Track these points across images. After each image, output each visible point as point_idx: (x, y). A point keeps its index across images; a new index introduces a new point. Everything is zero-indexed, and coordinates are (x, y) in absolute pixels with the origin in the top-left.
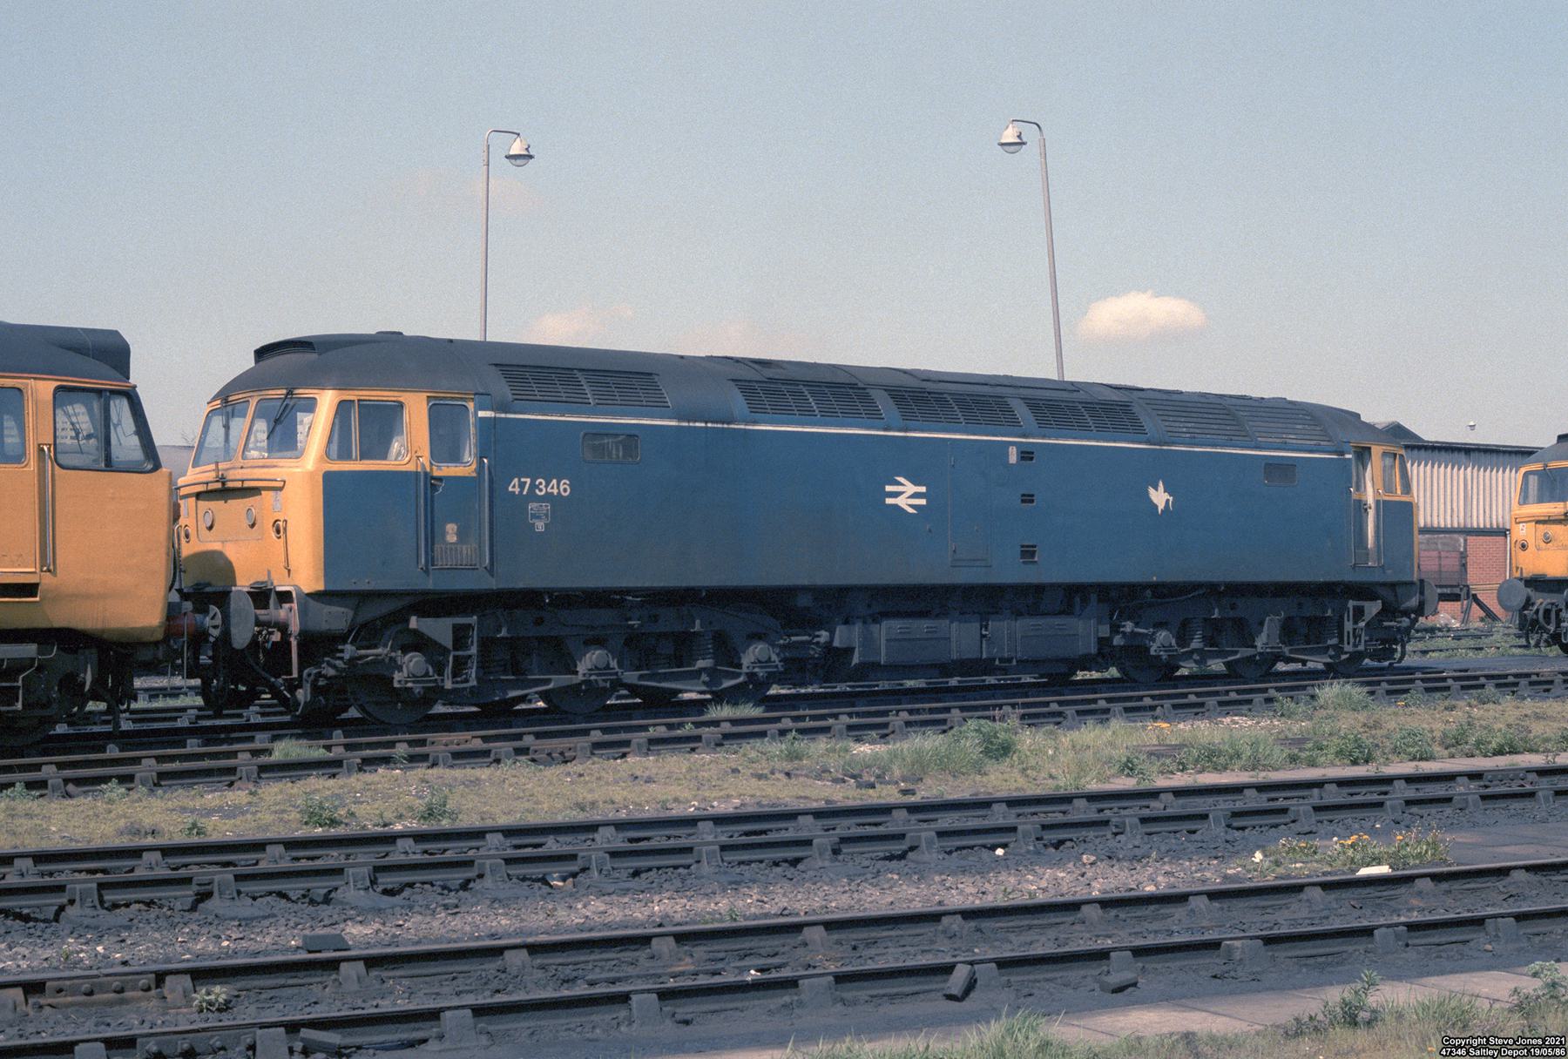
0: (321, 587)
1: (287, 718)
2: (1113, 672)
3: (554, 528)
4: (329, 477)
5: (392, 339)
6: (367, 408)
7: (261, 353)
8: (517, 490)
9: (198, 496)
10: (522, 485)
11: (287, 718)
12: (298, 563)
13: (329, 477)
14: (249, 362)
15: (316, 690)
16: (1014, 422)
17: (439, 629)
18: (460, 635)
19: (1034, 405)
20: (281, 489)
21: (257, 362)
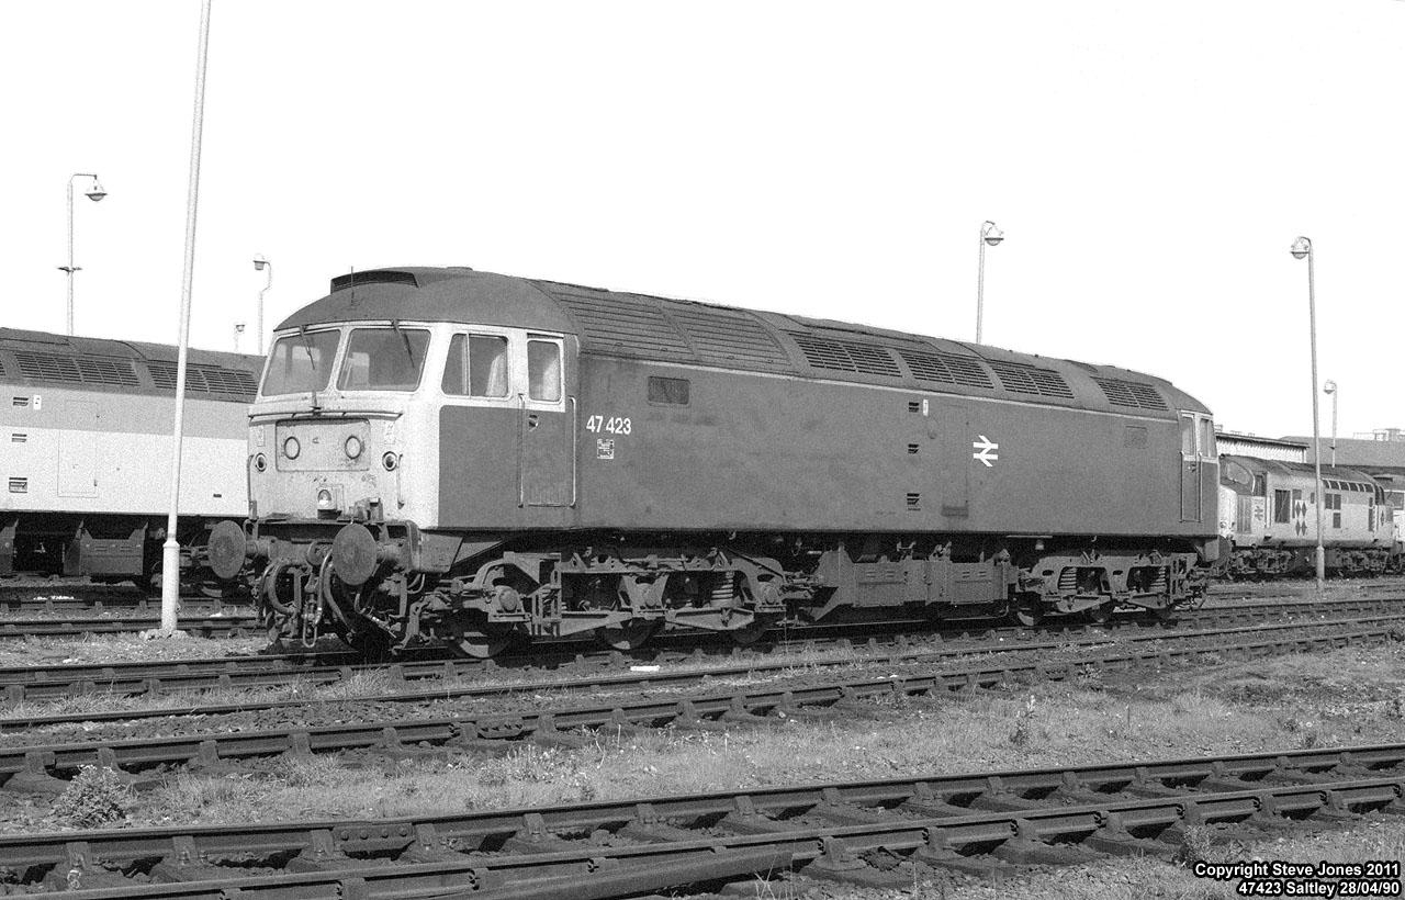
0: (436, 525)
1: (250, 646)
2: (253, 571)
3: (623, 467)
4: (446, 412)
5: (460, 276)
6: (475, 340)
7: (339, 283)
8: (593, 428)
9: (278, 423)
10: (597, 421)
11: (250, 646)
12: (416, 495)
13: (446, 412)
14: (325, 290)
15: (424, 626)
16: (895, 372)
17: (530, 564)
18: (546, 568)
19: (909, 358)
20: (395, 419)
21: (333, 290)
